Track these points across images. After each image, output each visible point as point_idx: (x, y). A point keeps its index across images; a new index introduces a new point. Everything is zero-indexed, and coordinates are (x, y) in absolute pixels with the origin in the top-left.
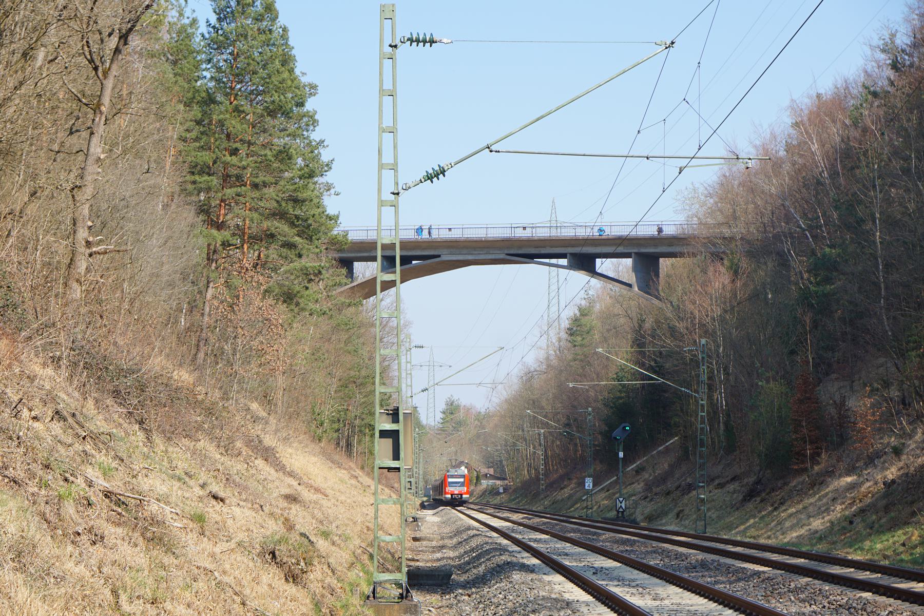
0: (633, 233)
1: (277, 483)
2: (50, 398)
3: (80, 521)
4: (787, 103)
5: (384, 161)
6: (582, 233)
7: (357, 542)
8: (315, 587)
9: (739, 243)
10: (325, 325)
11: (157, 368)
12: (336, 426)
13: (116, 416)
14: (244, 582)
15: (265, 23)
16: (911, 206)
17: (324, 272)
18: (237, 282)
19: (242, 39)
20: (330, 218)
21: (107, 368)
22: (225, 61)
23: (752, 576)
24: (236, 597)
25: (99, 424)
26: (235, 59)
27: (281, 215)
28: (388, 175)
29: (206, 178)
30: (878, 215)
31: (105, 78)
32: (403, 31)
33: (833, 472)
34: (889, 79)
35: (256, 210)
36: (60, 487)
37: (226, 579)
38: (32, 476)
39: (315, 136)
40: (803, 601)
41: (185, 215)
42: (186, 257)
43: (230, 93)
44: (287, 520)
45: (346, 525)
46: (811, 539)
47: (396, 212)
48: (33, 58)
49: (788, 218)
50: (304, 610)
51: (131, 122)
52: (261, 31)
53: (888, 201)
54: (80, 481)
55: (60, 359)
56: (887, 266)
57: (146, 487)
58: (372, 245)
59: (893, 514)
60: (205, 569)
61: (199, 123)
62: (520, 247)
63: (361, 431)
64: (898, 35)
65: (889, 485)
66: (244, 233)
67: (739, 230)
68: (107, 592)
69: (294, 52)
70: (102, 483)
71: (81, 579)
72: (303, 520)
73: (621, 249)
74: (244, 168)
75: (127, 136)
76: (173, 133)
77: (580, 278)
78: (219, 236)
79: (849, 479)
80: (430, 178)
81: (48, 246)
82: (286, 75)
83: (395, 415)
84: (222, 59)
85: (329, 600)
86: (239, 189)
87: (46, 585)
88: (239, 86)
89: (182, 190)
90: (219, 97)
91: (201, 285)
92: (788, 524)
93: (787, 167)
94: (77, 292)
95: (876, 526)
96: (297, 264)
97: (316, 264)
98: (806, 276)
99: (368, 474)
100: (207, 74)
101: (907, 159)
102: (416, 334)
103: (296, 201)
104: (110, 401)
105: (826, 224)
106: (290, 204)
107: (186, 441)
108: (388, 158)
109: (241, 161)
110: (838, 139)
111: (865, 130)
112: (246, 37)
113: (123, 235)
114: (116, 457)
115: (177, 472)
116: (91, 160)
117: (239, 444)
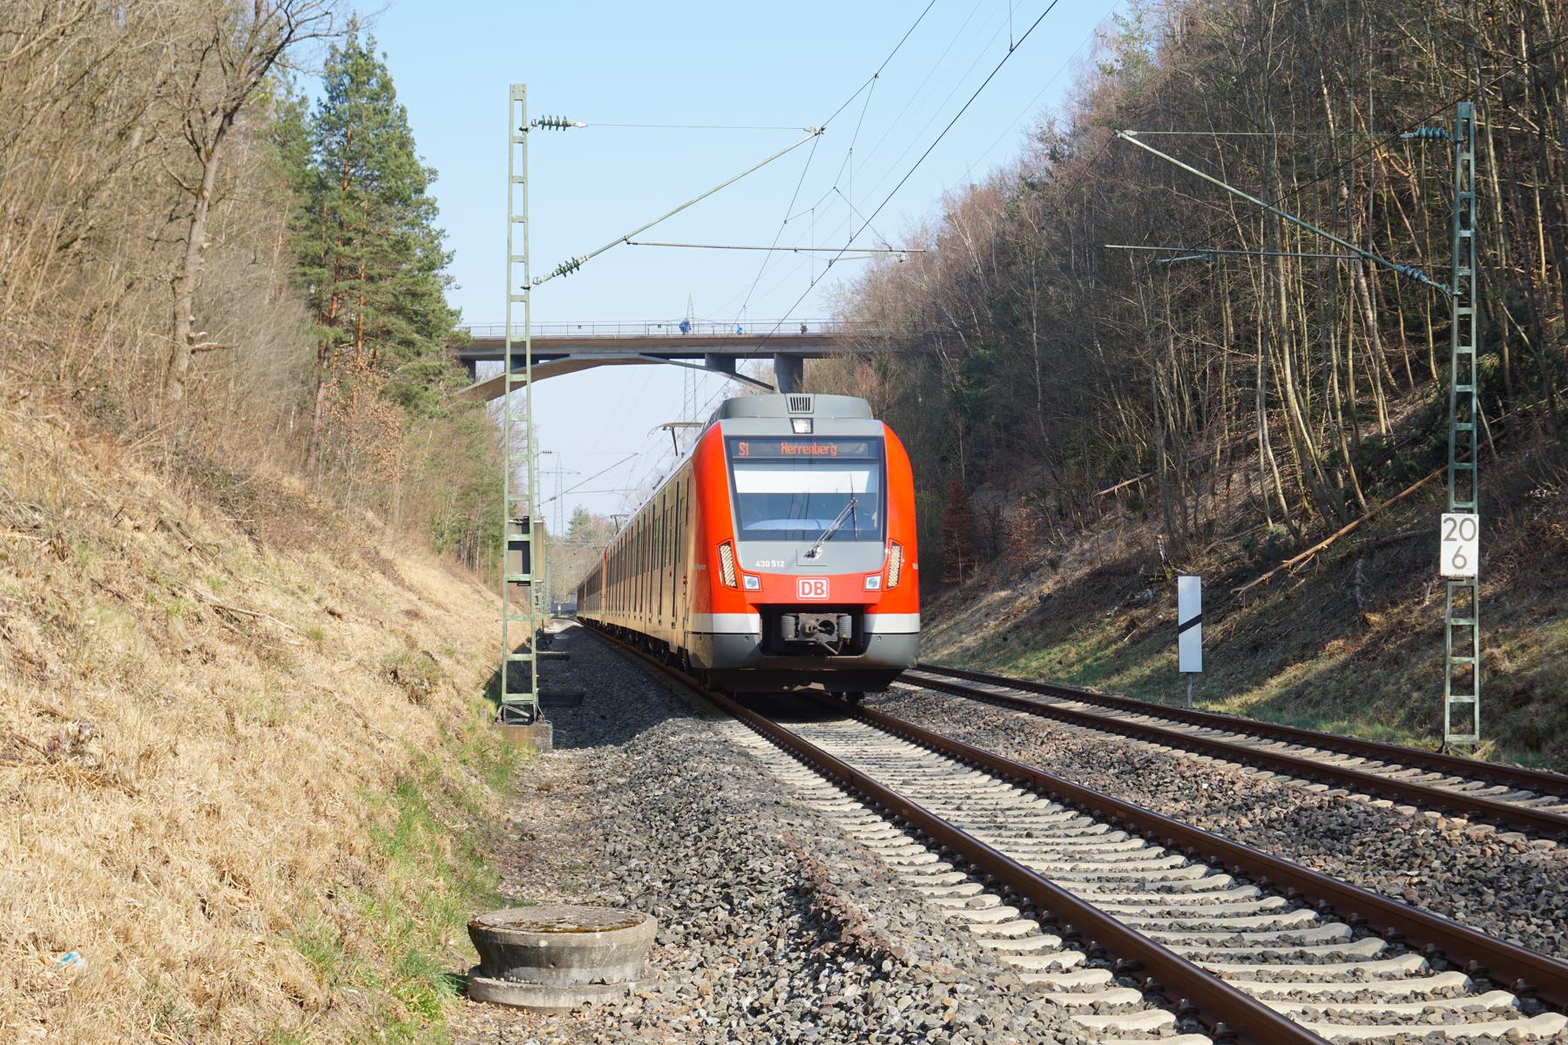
0: (776, 332)
1: (396, 598)
2: (153, 507)
3: (190, 638)
4: (938, 194)
5: (514, 253)
6: (720, 331)
7: (483, 661)
8: (440, 708)
9: (888, 343)
10: (445, 428)
11: (266, 475)
12: (456, 537)
13: (223, 526)
14: (366, 704)
15: (381, 103)
16: (1070, 306)
17: (445, 371)
18: (351, 382)
19: (356, 119)
20: (452, 314)
21: (213, 474)
22: (338, 143)
23: (903, 695)
24: (357, 720)
25: (206, 534)
26: (348, 142)
27: (398, 310)
28: (518, 268)
29: (317, 270)
30: (1034, 314)
31: (208, 160)
32: (535, 114)
33: (986, 586)
34: (1047, 170)
35: (372, 304)
36: (167, 602)
37: (349, 701)
38: (138, 590)
39: (435, 225)
40: (957, 722)
41: (294, 309)
42: (295, 355)
43: (343, 178)
44: (408, 637)
45: (471, 643)
46: (962, 657)
47: (527, 308)
48: (129, 138)
49: (940, 317)
50: (430, 733)
51: (236, 207)
52: (376, 112)
53: (1045, 299)
54: (189, 595)
55: (162, 464)
56: (1044, 368)
57: (259, 603)
58: (501, 343)
59: (1049, 631)
60: (324, 689)
61: (309, 210)
62: (655, 346)
63: (483, 542)
64: (1057, 123)
65: (1045, 599)
66: (358, 330)
67: (887, 329)
68: (222, 714)
69: (412, 135)
70: (211, 597)
71: (194, 701)
72: (427, 639)
73: (762, 349)
74: (358, 259)
75: (230, 224)
76: (282, 220)
77: (719, 379)
78: (331, 333)
79: (1003, 594)
80: (563, 271)
81: (147, 344)
82: (404, 159)
83: (525, 525)
84: (334, 141)
85: (455, 722)
86: (353, 282)
87: (156, 707)
88: (352, 171)
89: (291, 283)
90: (331, 183)
91: (312, 385)
92: (938, 641)
93: (939, 263)
94: (177, 392)
95: (1032, 642)
96: (416, 363)
97: (437, 363)
98: (958, 378)
99: (491, 588)
100: (318, 157)
101: (1066, 255)
102: (543, 439)
103: (414, 295)
104: (216, 509)
105: (980, 324)
106: (409, 298)
107: (298, 553)
108: (518, 250)
109: (355, 251)
110: (993, 233)
111: (1022, 224)
112: (360, 118)
113: (228, 331)
114: (225, 570)
115: (290, 586)
116: (193, 249)
117: (355, 556)
